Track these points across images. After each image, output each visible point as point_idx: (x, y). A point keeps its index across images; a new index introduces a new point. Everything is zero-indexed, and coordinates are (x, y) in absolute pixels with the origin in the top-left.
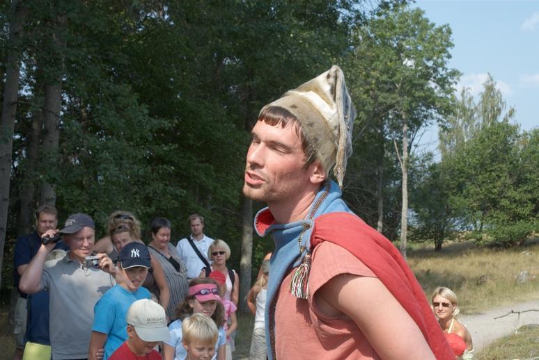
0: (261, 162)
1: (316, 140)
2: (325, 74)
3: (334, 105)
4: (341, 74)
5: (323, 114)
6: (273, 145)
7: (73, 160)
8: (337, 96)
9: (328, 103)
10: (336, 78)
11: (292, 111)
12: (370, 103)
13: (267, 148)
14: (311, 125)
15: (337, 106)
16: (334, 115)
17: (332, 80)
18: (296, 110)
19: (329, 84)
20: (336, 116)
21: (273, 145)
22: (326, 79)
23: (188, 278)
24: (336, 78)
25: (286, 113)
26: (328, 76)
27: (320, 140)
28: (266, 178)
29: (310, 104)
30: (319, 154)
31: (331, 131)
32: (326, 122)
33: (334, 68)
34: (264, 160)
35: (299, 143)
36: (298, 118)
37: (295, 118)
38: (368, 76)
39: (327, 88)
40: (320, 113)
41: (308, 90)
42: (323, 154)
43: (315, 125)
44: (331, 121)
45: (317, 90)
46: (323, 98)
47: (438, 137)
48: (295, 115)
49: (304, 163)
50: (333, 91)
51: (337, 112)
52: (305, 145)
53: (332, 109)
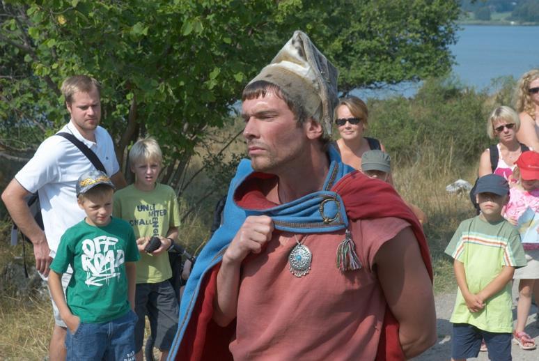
0: (256, 134)
1: (299, 97)
2: (290, 41)
3: (306, 64)
4: (305, 36)
5: (298, 73)
6: (261, 116)
7: (264, 127)
8: (307, 56)
9: (300, 64)
10: (301, 42)
11: (267, 80)
12: (282, 14)
13: (258, 120)
14: (289, 85)
15: (309, 64)
16: (309, 72)
17: (297, 44)
18: (271, 78)
19: (296, 48)
20: (311, 71)
21: (261, 116)
22: (291, 46)
23: (431, 23)
24: (301, 42)
25: (263, 84)
26: (293, 42)
27: (303, 96)
28: (266, 148)
29: (284, 69)
30: (307, 109)
31: (311, 86)
32: (300, 77)
33: (296, 34)
34: (258, 131)
35: (283, 103)
36: (275, 83)
37: (272, 85)
38: (397, 110)
39: (295, 52)
40: (295, 74)
41: (279, 61)
42: (311, 108)
43: (293, 84)
44: (308, 76)
45: (287, 57)
46: (294, 62)
47: (170, 327)
48: (272, 81)
49: (296, 121)
50: (302, 53)
51: (311, 68)
52: (290, 105)
53: (305, 67)
